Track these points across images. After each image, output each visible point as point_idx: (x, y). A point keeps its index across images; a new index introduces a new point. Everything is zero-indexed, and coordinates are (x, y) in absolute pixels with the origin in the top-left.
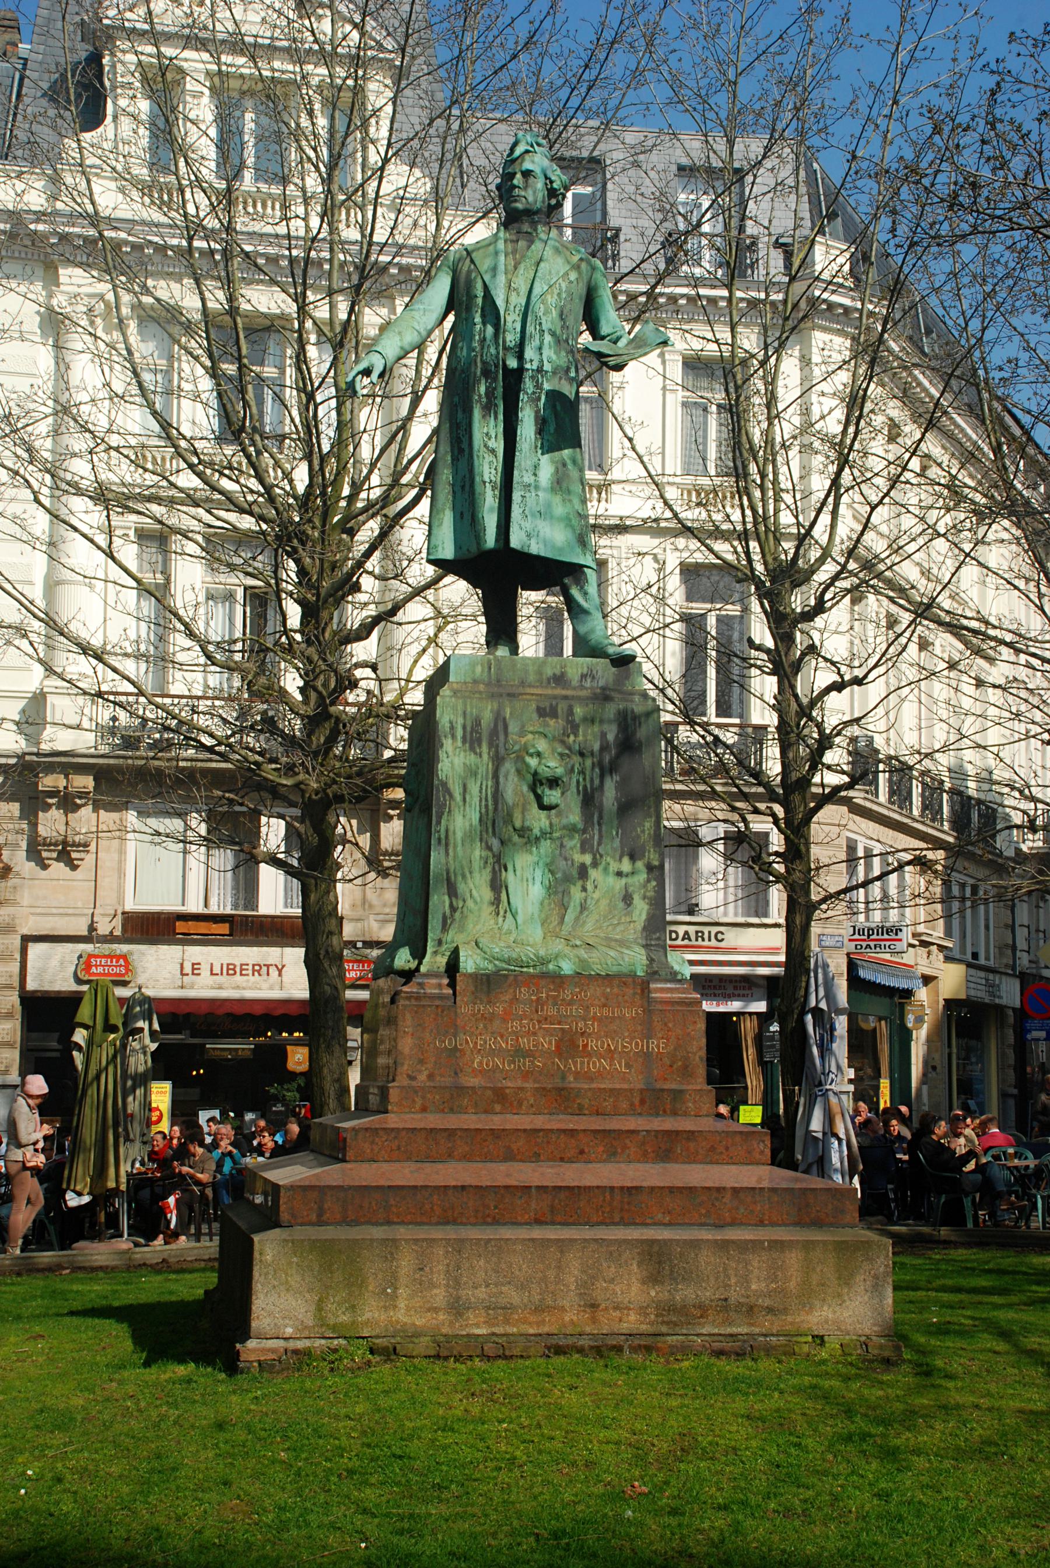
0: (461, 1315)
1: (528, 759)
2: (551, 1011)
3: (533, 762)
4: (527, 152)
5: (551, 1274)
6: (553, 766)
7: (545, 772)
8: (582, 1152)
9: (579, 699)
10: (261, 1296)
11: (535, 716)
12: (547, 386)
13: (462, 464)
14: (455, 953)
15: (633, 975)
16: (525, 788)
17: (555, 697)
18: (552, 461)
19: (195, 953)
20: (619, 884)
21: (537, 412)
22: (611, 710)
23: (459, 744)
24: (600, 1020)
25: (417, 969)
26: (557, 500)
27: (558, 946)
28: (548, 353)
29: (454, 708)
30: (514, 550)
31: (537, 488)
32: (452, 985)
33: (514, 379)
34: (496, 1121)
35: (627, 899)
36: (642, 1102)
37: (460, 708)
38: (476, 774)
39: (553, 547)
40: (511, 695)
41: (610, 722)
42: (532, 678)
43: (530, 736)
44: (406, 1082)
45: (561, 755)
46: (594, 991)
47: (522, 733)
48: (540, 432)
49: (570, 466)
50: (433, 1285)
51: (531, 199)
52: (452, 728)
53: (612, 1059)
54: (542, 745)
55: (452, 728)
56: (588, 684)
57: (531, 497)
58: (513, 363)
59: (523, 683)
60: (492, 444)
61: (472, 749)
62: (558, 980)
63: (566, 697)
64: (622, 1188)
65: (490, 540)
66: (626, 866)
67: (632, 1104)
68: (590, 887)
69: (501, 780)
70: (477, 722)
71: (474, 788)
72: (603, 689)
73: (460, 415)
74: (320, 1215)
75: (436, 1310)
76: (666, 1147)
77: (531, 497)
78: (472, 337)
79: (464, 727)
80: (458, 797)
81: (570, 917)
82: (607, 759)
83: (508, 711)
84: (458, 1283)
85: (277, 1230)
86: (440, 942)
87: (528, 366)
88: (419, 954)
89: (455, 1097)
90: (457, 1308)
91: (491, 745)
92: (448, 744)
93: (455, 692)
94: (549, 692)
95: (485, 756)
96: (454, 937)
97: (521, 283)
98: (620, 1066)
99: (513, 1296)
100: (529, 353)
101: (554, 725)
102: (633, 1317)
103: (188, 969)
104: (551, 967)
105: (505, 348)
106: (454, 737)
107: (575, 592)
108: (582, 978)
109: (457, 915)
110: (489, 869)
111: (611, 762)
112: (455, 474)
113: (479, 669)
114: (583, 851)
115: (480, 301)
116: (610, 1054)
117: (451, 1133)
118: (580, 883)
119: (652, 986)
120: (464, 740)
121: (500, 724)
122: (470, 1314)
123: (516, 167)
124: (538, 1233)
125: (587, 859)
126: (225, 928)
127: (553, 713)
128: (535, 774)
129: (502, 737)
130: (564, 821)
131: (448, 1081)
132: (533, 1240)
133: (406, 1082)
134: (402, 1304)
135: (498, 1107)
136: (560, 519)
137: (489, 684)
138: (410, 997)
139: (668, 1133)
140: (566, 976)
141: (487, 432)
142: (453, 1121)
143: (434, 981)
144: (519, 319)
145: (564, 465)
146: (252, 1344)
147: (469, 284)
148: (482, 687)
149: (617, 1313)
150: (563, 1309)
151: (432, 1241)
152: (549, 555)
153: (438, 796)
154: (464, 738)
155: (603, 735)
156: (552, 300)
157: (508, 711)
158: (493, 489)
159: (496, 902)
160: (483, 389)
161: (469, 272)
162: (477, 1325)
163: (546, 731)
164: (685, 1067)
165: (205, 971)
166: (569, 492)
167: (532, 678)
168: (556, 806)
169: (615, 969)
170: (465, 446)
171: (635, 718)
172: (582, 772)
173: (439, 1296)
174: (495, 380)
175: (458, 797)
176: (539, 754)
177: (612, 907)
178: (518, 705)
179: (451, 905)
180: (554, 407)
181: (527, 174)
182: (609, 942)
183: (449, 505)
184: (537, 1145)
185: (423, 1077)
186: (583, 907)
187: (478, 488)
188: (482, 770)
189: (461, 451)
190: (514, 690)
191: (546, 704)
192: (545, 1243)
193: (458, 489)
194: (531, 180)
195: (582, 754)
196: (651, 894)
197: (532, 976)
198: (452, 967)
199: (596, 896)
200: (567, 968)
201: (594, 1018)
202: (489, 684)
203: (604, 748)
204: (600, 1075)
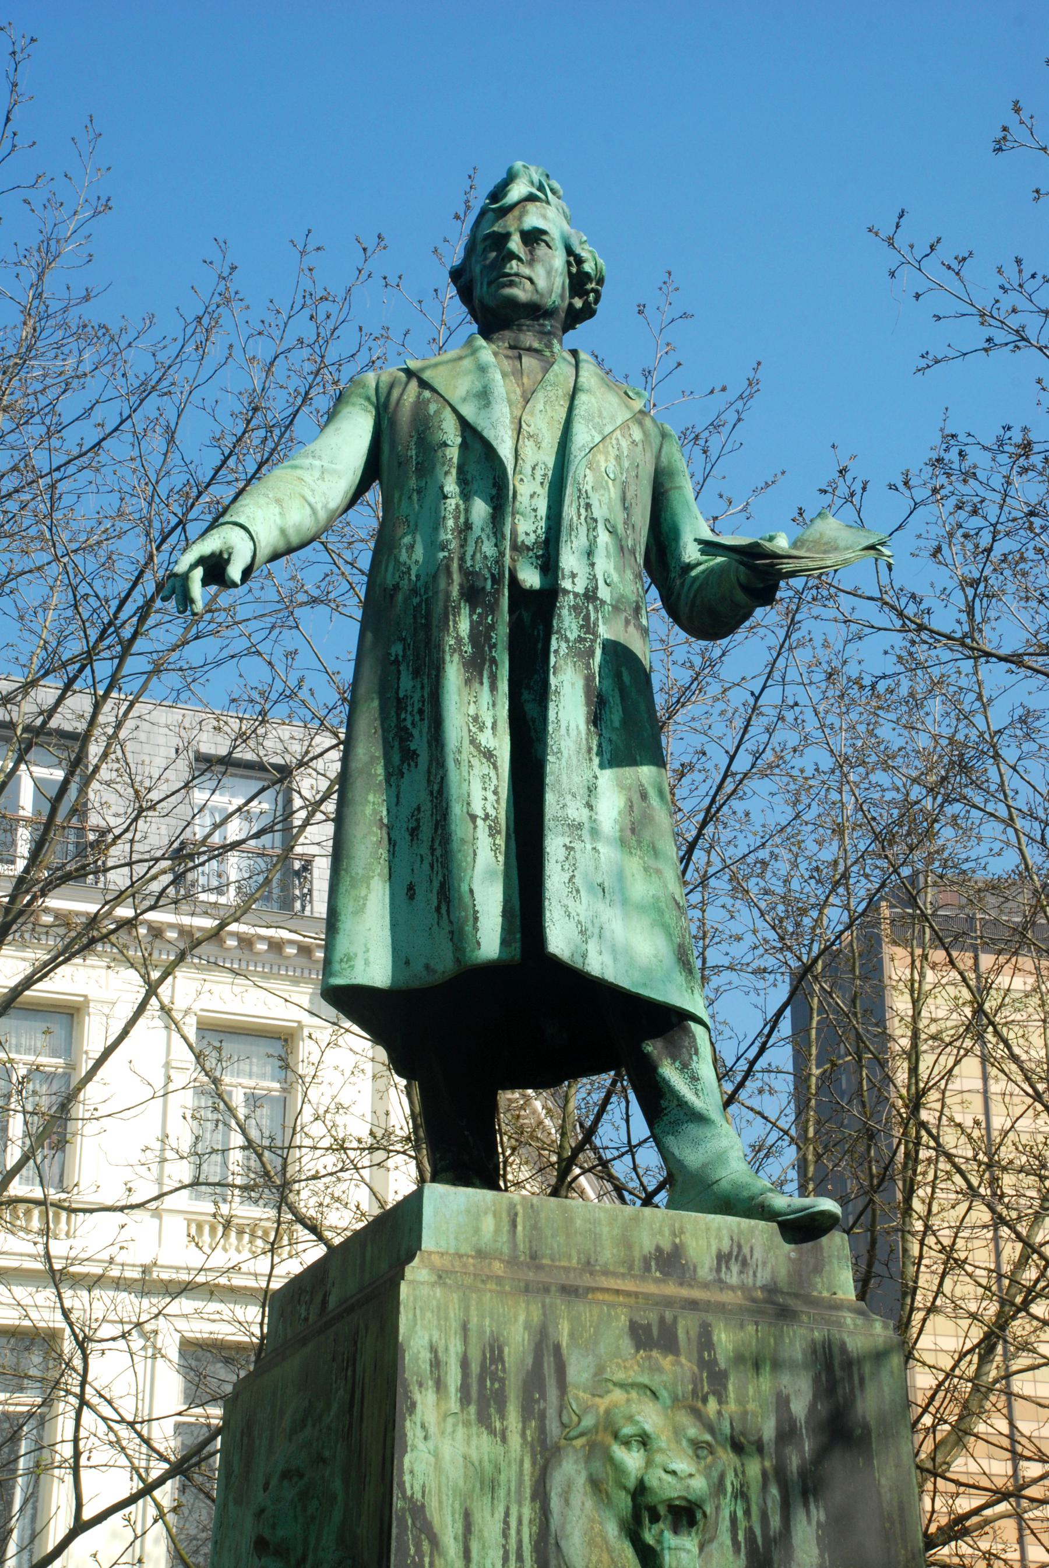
1: (619, 1452)
3: (632, 1460)
4: (531, 198)
6: (679, 1473)
7: (666, 1487)
9: (721, 1309)
11: (626, 1345)
12: (604, 632)
13: (415, 781)
16: (612, 1530)
17: (668, 1302)
18: (621, 785)
21: (589, 679)
22: (796, 1342)
26: (634, 865)
28: (605, 565)
29: (441, 1312)
30: (555, 962)
31: (595, 832)
37: (454, 1314)
38: (492, 1486)
39: (631, 962)
41: (793, 1366)
43: (618, 1395)
45: (697, 1446)
47: (600, 1383)
48: (596, 719)
49: (654, 800)
51: (542, 283)
52: (436, 1363)
54: (650, 1417)
55: (436, 1363)
56: (733, 1277)
57: (584, 849)
58: (531, 578)
59: (588, 1266)
60: (486, 739)
61: (484, 1420)
63: (693, 1305)
65: (489, 939)
69: (555, 1503)
70: (495, 1352)
71: (489, 1525)
72: (771, 1290)
73: (406, 683)
77: (584, 849)
78: (438, 523)
79: (465, 1364)
80: (452, 1548)
82: (794, 1463)
87: (566, 584)
91: (527, 1411)
93: (441, 1276)
94: (652, 1288)
95: (515, 1440)
97: (544, 423)
100: (570, 560)
101: (675, 1370)
105: (515, 547)
106: (439, 1385)
107: (669, 1072)
111: (803, 1474)
112: (395, 802)
113: (488, 1225)
120: (465, 1399)
121: (548, 1358)
123: (510, 223)
127: (668, 1342)
128: (641, 1489)
129: (552, 1393)
136: (641, 909)
137: (512, 1262)
141: (475, 716)
144: (543, 492)
145: (644, 796)
148: (498, 1268)
152: (625, 982)
154: (464, 1389)
155: (782, 1402)
156: (606, 462)
158: (493, 832)
160: (464, 626)
161: (420, 405)
163: (655, 1381)
166: (655, 852)
167: (608, 1254)
170: (419, 743)
171: (850, 1363)
172: (741, 1494)
174: (493, 608)
175: (452, 1548)
176: (644, 1440)
178: (587, 1312)
180: (618, 676)
181: (533, 237)
183: (381, 868)
187: (459, 827)
188: (508, 1476)
189: (409, 756)
190: (572, 1280)
193: (403, 837)
194: (541, 250)
195: (738, 1447)
202: (512, 1262)
203: (787, 1433)
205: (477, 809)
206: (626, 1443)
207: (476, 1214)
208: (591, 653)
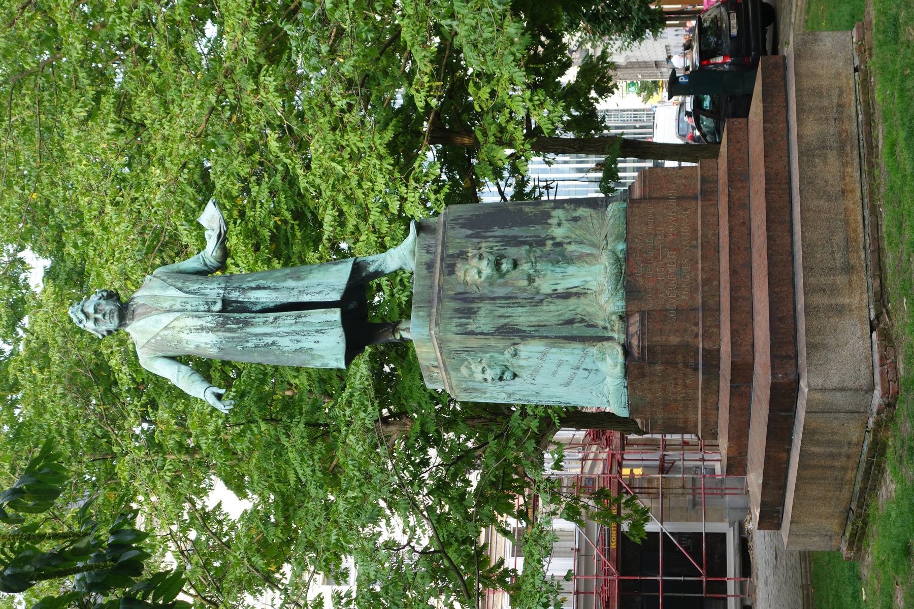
0: (853, 267)
5: (824, 216)
8: (744, 223)
11: (453, 276)
15: (626, 210)
17: (441, 266)
20: (566, 225)
29: (447, 324)
30: (342, 298)
35: (576, 219)
42: (428, 282)
52: (460, 325)
55: (460, 325)
60: (270, 319)
61: (475, 313)
62: (628, 253)
66: (553, 221)
68: (568, 240)
70: (457, 310)
71: (502, 311)
74: (791, 358)
80: (507, 320)
81: (587, 250)
83: (450, 292)
90: (848, 269)
94: (438, 270)
95: (480, 305)
102: (849, 170)
106: (466, 324)
107: (371, 269)
108: (627, 238)
109: (586, 318)
110: (555, 300)
113: (421, 313)
114: (545, 245)
118: (565, 246)
120: (470, 318)
122: (852, 262)
125: (549, 243)
135: (715, 283)
140: (627, 246)
149: (847, 179)
154: (467, 318)
157: (450, 292)
159: (578, 295)
162: (859, 257)
167: (428, 282)
169: (622, 219)
173: (841, 280)
174: (228, 318)
175: (507, 320)
177: (581, 228)
179: (580, 322)
186: (581, 243)
191: (446, 270)
196: (572, 206)
200: (621, 246)
207: (418, 317)
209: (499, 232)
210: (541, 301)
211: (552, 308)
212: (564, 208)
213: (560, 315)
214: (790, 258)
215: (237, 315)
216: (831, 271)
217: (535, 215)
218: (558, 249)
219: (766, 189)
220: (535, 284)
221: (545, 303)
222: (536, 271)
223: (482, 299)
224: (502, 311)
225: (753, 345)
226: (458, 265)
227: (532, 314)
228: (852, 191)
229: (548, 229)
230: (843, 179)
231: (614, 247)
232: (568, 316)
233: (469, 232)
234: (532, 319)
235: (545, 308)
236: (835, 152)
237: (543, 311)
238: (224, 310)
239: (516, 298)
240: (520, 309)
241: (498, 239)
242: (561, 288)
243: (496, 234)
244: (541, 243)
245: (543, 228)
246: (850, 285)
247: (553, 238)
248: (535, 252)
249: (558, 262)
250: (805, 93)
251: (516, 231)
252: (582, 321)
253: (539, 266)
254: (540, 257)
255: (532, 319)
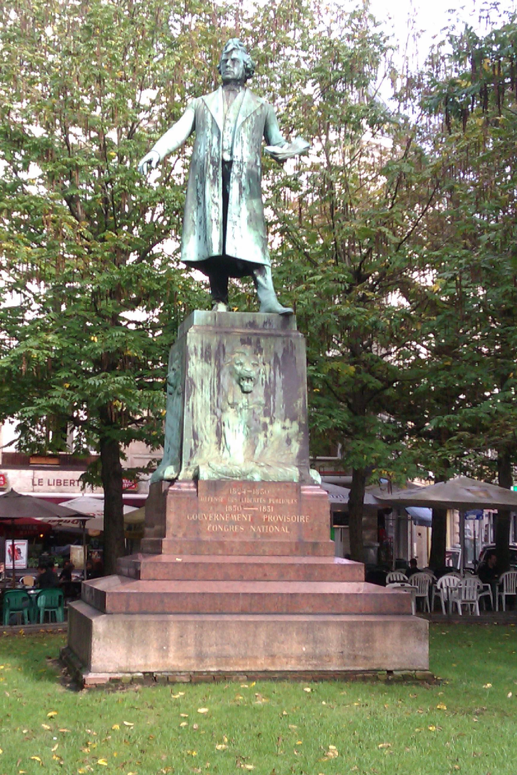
2: (248, 501)
3: (239, 368)
4: (234, 49)
5: (251, 639)
8: (265, 575)
10: (97, 650)
11: (240, 343)
14: (198, 468)
15: (292, 482)
16: (234, 382)
19: (40, 474)
20: (284, 433)
23: (199, 358)
24: (274, 506)
25: (177, 478)
27: (251, 466)
29: (197, 339)
32: (196, 486)
33: (227, 166)
34: (219, 559)
35: (289, 441)
36: (297, 548)
37: (200, 339)
38: (208, 374)
40: (227, 333)
42: (238, 323)
44: (171, 538)
46: (270, 491)
50: (187, 645)
53: (281, 526)
55: (195, 349)
58: (227, 158)
59: (233, 326)
60: (216, 200)
61: (206, 361)
62: (252, 484)
63: (256, 334)
64: (288, 594)
66: (287, 423)
67: (291, 551)
68: (268, 435)
70: (209, 347)
71: (207, 382)
75: (190, 658)
76: (309, 574)
79: (202, 350)
80: (199, 387)
81: (258, 451)
84: (201, 643)
85: (105, 616)
86: (189, 464)
87: (235, 159)
88: (179, 470)
89: (197, 546)
90: (201, 657)
92: (193, 358)
93: (197, 331)
95: (213, 365)
96: (196, 461)
98: (285, 530)
99: (230, 651)
100: (236, 152)
103: (36, 482)
104: (248, 477)
106: (196, 354)
107: (259, 278)
109: (198, 449)
110: (215, 425)
113: (209, 318)
114: (265, 416)
115: (210, 125)
116: (280, 524)
117: (195, 565)
118: (263, 433)
119: (302, 487)
124: (243, 618)
125: (267, 420)
126: (56, 461)
130: (255, 400)
131: (193, 537)
132: (241, 621)
133: (171, 538)
134: (171, 655)
135: (220, 552)
137: (215, 326)
138: (173, 492)
139: (310, 565)
142: (197, 559)
143: (186, 484)
146: (91, 675)
147: (204, 116)
149: (285, 660)
150: (256, 658)
151: (188, 621)
153: (188, 385)
159: (219, 442)
160: (211, 171)
162: (212, 666)
164: (319, 530)
165: (45, 484)
167: (238, 323)
168: (251, 392)
170: (201, 201)
172: (265, 373)
173: (191, 650)
174: (218, 166)
175: (199, 387)
176: (241, 364)
177: (280, 445)
180: (249, 181)
182: (279, 464)
184: (242, 573)
185: (180, 535)
186: (265, 445)
191: (245, 337)
192: (247, 623)
197: (238, 482)
198: (196, 478)
199: (272, 439)
200: (257, 477)
201: (271, 505)
202: (215, 326)
204: (275, 534)
205: (213, 219)
206: (237, 364)
207: (206, 316)
208: (241, 177)
209: (279, 379)
210: (215, 414)
211: (209, 422)
212: (300, 431)
213: (202, 429)
214: (217, 611)
215: (220, 173)
216: (199, 643)
217: (294, 408)
218: (261, 427)
219: (282, 594)
220: (229, 409)
221: (213, 416)
222: (241, 409)
223: (219, 368)
224: (207, 382)
225: (154, 580)
226: (249, 347)
227: (204, 406)
228: (273, 664)
229: (281, 419)
230: (285, 656)
231: (256, 471)
232: (201, 435)
233: (280, 356)
234: (199, 407)
235: (209, 416)
236: (311, 650)
237: (206, 415)
238: (224, 162)
239: (219, 393)
240: (208, 397)
241: (272, 379)
242: (226, 429)
243: (278, 378)
244: (267, 413)
245: (281, 415)
246: (186, 658)
247: (272, 423)
248: (259, 408)
249: (248, 427)
250: (367, 628)
251: (280, 393)
252: (196, 446)
253: (245, 412)
254: (254, 413)
255: (199, 407)
